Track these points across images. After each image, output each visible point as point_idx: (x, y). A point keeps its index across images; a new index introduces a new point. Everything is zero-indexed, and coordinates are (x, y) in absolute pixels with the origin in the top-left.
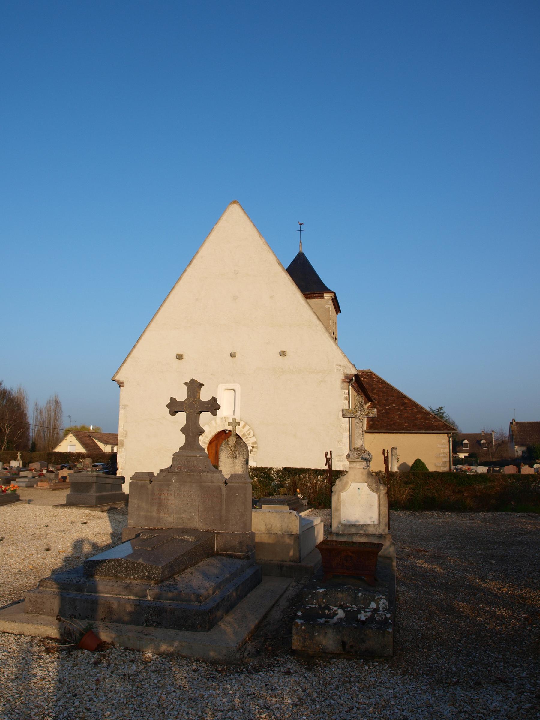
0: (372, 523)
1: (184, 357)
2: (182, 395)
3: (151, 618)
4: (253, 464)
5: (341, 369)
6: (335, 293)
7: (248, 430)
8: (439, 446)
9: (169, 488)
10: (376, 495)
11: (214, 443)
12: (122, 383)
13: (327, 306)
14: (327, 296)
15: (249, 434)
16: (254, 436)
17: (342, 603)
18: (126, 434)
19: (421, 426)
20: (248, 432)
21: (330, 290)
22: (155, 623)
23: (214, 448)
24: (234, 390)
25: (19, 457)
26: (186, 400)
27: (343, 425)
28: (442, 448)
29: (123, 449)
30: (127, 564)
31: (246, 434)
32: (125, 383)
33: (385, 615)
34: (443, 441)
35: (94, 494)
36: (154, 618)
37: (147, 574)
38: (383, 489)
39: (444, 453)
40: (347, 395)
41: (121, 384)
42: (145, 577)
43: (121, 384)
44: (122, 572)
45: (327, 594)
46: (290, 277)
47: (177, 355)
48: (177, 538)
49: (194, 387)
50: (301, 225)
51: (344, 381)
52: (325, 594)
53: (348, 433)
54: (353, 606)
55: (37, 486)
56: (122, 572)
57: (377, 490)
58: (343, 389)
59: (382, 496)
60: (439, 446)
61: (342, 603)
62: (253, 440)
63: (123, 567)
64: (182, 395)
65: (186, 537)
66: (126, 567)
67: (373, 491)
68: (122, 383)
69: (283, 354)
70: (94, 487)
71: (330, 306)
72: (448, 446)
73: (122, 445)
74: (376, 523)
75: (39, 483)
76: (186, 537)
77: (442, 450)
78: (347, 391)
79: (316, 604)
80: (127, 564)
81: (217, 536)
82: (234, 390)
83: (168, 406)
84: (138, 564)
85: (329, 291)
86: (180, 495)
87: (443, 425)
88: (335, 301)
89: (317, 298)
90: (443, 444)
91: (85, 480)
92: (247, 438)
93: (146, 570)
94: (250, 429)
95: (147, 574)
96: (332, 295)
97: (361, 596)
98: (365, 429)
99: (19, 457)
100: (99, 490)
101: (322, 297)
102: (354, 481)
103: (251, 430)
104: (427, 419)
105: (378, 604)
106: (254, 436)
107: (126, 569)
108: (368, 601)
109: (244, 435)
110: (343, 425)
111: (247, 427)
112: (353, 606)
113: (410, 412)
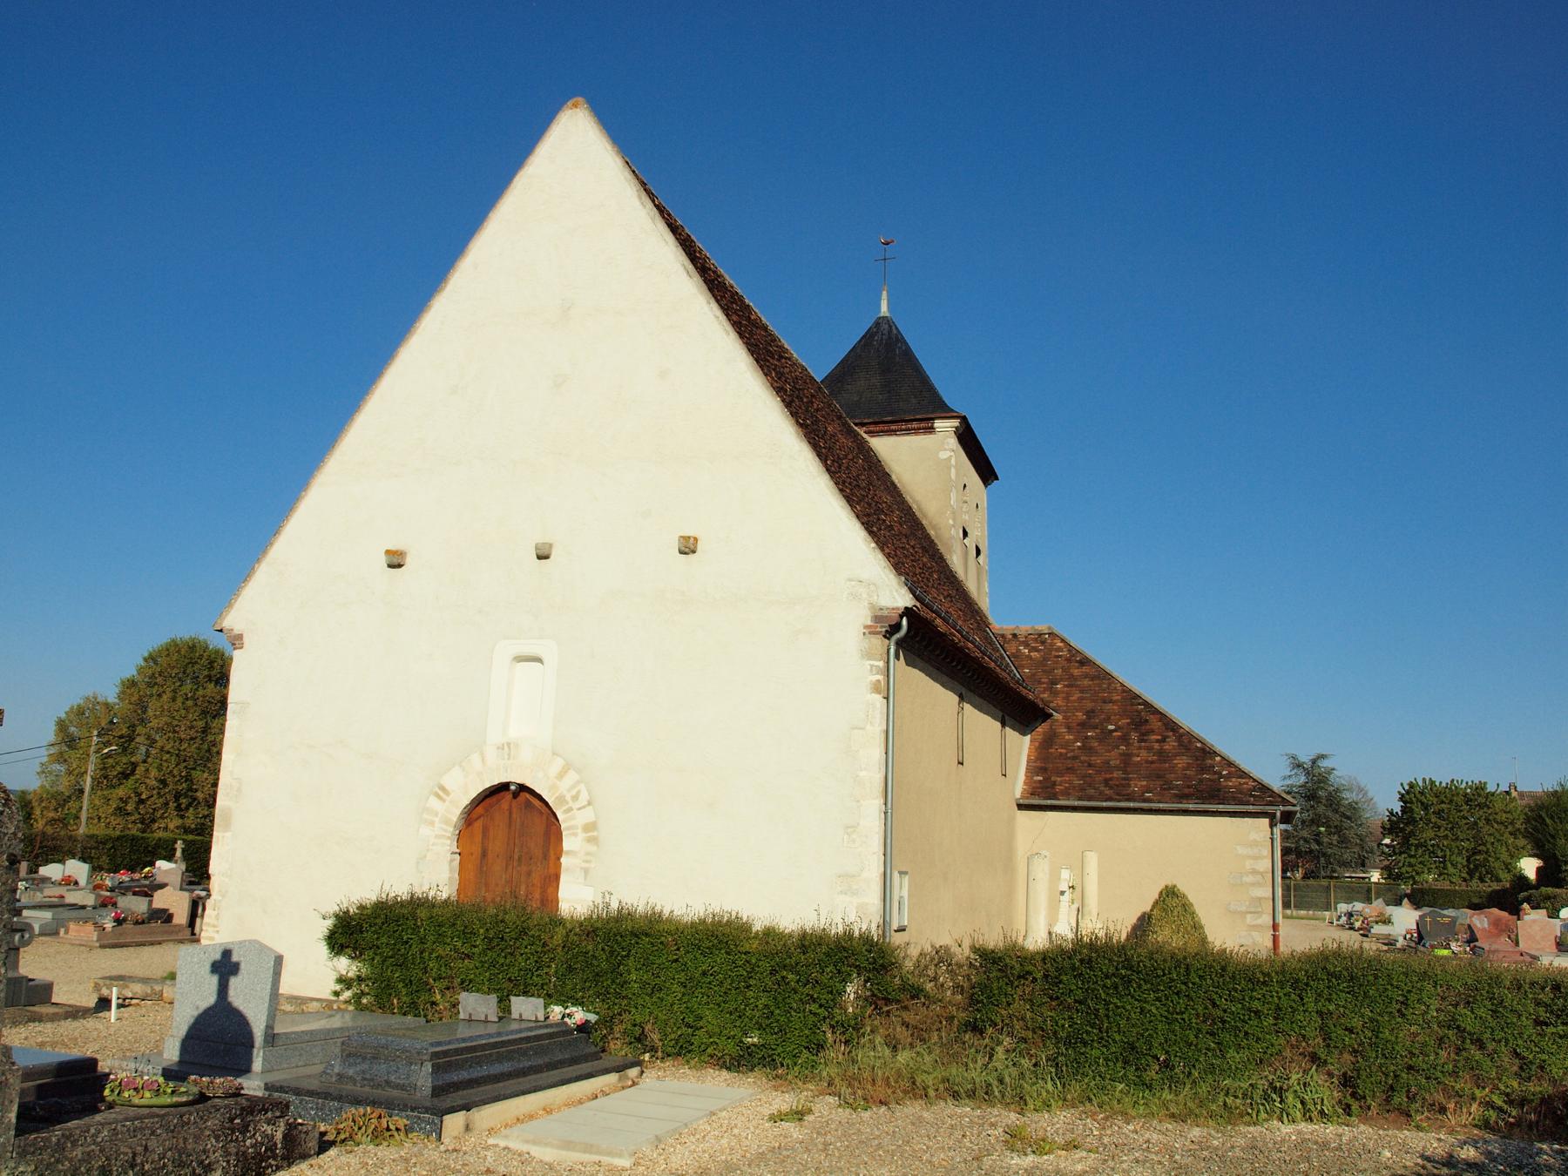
1: (408, 560)
4: (155, 905)
6: (964, 419)
7: (573, 787)
8: (1241, 850)
11: (478, 825)
12: (240, 637)
13: (944, 455)
14: (946, 427)
15: (575, 798)
16: (589, 803)
19: (1186, 791)
20: (574, 792)
23: (478, 838)
25: (179, 854)
27: (862, 774)
28: (1249, 857)
29: (228, 834)
31: (568, 798)
32: (246, 640)
34: (1253, 836)
39: (1254, 872)
47: (388, 552)
51: (870, 631)
55: (67, 932)
58: (868, 655)
60: (1241, 850)
62: (587, 816)
68: (240, 637)
72: (1266, 852)
75: (72, 926)
77: (1248, 864)
82: (539, 660)
85: (945, 412)
88: (968, 440)
89: (916, 431)
90: (1255, 844)
92: (571, 809)
94: (578, 782)
96: (956, 423)
98: (1018, 795)
99: (179, 854)
101: (931, 430)
103: (582, 787)
104: (1203, 769)
106: (589, 803)
110: (862, 774)
111: (572, 777)
113: (1156, 746)
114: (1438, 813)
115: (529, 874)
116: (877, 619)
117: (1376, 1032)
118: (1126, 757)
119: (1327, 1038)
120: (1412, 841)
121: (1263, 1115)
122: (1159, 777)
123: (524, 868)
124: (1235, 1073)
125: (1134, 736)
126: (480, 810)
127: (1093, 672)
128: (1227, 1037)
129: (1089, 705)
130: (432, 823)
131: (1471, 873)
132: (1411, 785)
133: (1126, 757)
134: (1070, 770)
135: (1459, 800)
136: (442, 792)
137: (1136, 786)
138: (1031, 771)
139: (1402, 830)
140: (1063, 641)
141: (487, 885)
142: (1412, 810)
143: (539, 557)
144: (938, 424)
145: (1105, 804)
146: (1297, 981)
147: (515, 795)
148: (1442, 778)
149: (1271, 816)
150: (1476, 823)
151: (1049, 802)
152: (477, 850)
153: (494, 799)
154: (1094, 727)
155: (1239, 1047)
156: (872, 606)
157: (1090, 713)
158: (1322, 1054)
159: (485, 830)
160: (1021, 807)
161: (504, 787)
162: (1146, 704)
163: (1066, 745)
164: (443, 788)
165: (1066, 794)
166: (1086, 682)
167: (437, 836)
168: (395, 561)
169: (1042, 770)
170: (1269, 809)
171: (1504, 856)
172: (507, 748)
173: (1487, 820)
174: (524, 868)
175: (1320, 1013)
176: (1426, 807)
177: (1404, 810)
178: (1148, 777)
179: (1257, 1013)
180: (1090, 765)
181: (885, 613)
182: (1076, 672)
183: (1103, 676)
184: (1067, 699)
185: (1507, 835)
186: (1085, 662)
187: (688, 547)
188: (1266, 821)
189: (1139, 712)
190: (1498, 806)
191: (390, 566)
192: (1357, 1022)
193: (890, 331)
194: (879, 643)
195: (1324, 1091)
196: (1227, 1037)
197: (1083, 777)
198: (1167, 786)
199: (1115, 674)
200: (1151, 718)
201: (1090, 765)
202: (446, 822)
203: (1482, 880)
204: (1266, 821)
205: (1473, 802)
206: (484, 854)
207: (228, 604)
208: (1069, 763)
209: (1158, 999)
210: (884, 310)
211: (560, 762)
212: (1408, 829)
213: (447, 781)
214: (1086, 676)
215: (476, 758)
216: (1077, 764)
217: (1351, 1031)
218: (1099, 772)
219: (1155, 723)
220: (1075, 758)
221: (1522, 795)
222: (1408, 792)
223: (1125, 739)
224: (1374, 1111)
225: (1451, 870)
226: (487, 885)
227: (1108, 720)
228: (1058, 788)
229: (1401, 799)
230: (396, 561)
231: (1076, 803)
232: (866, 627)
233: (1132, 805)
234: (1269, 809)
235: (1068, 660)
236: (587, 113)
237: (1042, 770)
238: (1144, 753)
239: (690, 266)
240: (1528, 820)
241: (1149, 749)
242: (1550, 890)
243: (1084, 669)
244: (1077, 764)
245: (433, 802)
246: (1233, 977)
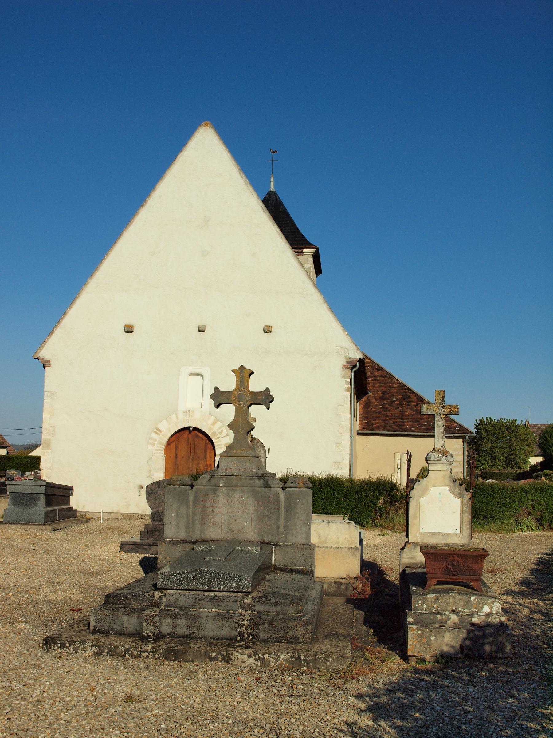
0: (454, 532)
1: (135, 329)
2: (229, 384)
3: (246, 631)
5: (342, 351)
6: (317, 249)
7: (220, 428)
9: (215, 493)
10: (458, 501)
11: (173, 445)
12: (49, 361)
15: (221, 433)
16: (227, 435)
17: (454, 608)
18: (54, 431)
20: (220, 431)
21: (311, 245)
22: (251, 637)
23: (173, 450)
24: (201, 375)
26: (234, 390)
27: (343, 423)
29: (50, 451)
30: (211, 574)
31: (217, 433)
32: (52, 363)
33: (500, 618)
34: (456, 446)
35: (41, 508)
36: (249, 631)
37: (234, 585)
38: (467, 496)
40: (349, 385)
41: (45, 364)
42: (232, 588)
43: (45, 364)
44: (205, 583)
45: (437, 599)
46: (278, 230)
47: (126, 326)
48: (239, 550)
49: (243, 374)
50: (273, 152)
51: (345, 367)
52: (423, 603)
53: (349, 434)
54: (465, 610)
56: (205, 583)
57: (460, 496)
59: (465, 501)
61: (454, 608)
63: (205, 578)
64: (229, 384)
65: (249, 548)
66: (209, 578)
67: (455, 496)
68: (49, 361)
69: (268, 330)
70: (42, 499)
71: (310, 264)
72: (461, 453)
73: (48, 445)
74: (458, 531)
76: (249, 548)
78: (349, 380)
79: (426, 610)
80: (211, 574)
81: (275, 548)
82: (201, 375)
83: (212, 397)
84: (224, 574)
85: (309, 245)
86: (228, 502)
87: (456, 427)
88: (316, 258)
91: (29, 490)
92: (219, 438)
93: (234, 580)
94: (222, 426)
95: (234, 585)
96: (314, 251)
97: (474, 600)
100: (48, 503)
102: (435, 485)
105: (491, 608)
106: (227, 435)
107: (210, 580)
108: (481, 605)
109: (214, 434)
110: (343, 423)
112: (465, 610)
113: (415, 408)
114: (492, 435)
115: (198, 464)
116: (348, 362)
117: (548, 505)
118: (402, 412)
119: (533, 507)
120: (480, 448)
121: (516, 530)
122: (418, 421)
123: (196, 462)
124: (506, 519)
125: (405, 403)
126: (174, 438)
127: (384, 374)
128: (504, 508)
129: (384, 389)
130: (154, 444)
131: (507, 465)
132: (481, 421)
133: (402, 412)
134: (379, 418)
135: (503, 428)
136: (158, 431)
137: (408, 425)
138: (362, 418)
139: (476, 443)
140: (369, 359)
141: (178, 469)
142: (481, 433)
143: (200, 331)
144: (305, 251)
145: (395, 433)
146: (526, 491)
147: (190, 432)
148: (496, 417)
149: (464, 438)
150: (511, 440)
151: (371, 432)
152: (173, 455)
153: (180, 433)
154: (386, 399)
155: (508, 511)
156: (346, 358)
157: (384, 393)
158: (532, 512)
159: (177, 449)
160: (358, 434)
161: (187, 428)
162: (408, 389)
163: (375, 406)
164: (158, 429)
165: (378, 428)
166: (381, 378)
167: (156, 450)
168: (130, 330)
169: (366, 418)
170: (463, 435)
171: (523, 456)
172: (188, 412)
173: (516, 438)
174: (196, 462)
175: (532, 500)
176: (487, 431)
177: (477, 433)
178: (412, 421)
179: (514, 500)
180: (387, 416)
181: (352, 360)
182: (376, 374)
183: (388, 376)
184: (373, 386)
185: (525, 446)
186: (380, 369)
187: (268, 330)
188: (461, 440)
189: (406, 392)
190: (522, 431)
191: (126, 332)
192: (542, 503)
193: (276, 199)
194: (348, 371)
195: (532, 523)
196: (504, 508)
197: (385, 421)
198: (421, 425)
199: (394, 375)
200: (411, 395)
201: (387, 416)
202: (161, 444)
203: (512, 468)
204: (461, 440)
205: (509, 428)
206: (176, 457)
207: (41, 346)
208: (378, 415)
209: (484, 497)
210: (272, 187)
211: (212, 419)
212: (479, 443)
213: (160, 426)
214: (381, 376)
215: (173, 417)
216: (381, 415)
217: (540, 505)
218: (390, 419)
219: (413, 398)
220: (380, 412)
221: (531, 425)
222: (479, 424)
223: (401, 404)
224: (546, 528)
225: (498, 463)
226: (178, 469)
227: (392, 396)
228: (374, 426)
229: (476, 428)
230: (129, 330)
231: (383, 432)
232: (343, 366)
233: (407, 433)
234: (463, 435)
235: (372, 368)
236: (212, 130)
237: (366, 418)
238: (409, 411)
239: (265, 208)
240: (540, 438)
241: (412, 409)
242: (548, 471)
243: (380, 372)
244: (381, 415)
245: (154, 435)
246: (507, 490)
